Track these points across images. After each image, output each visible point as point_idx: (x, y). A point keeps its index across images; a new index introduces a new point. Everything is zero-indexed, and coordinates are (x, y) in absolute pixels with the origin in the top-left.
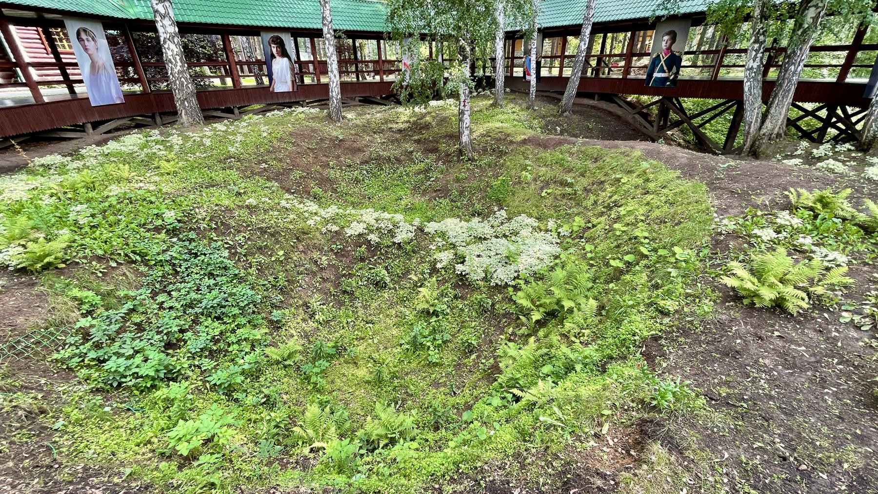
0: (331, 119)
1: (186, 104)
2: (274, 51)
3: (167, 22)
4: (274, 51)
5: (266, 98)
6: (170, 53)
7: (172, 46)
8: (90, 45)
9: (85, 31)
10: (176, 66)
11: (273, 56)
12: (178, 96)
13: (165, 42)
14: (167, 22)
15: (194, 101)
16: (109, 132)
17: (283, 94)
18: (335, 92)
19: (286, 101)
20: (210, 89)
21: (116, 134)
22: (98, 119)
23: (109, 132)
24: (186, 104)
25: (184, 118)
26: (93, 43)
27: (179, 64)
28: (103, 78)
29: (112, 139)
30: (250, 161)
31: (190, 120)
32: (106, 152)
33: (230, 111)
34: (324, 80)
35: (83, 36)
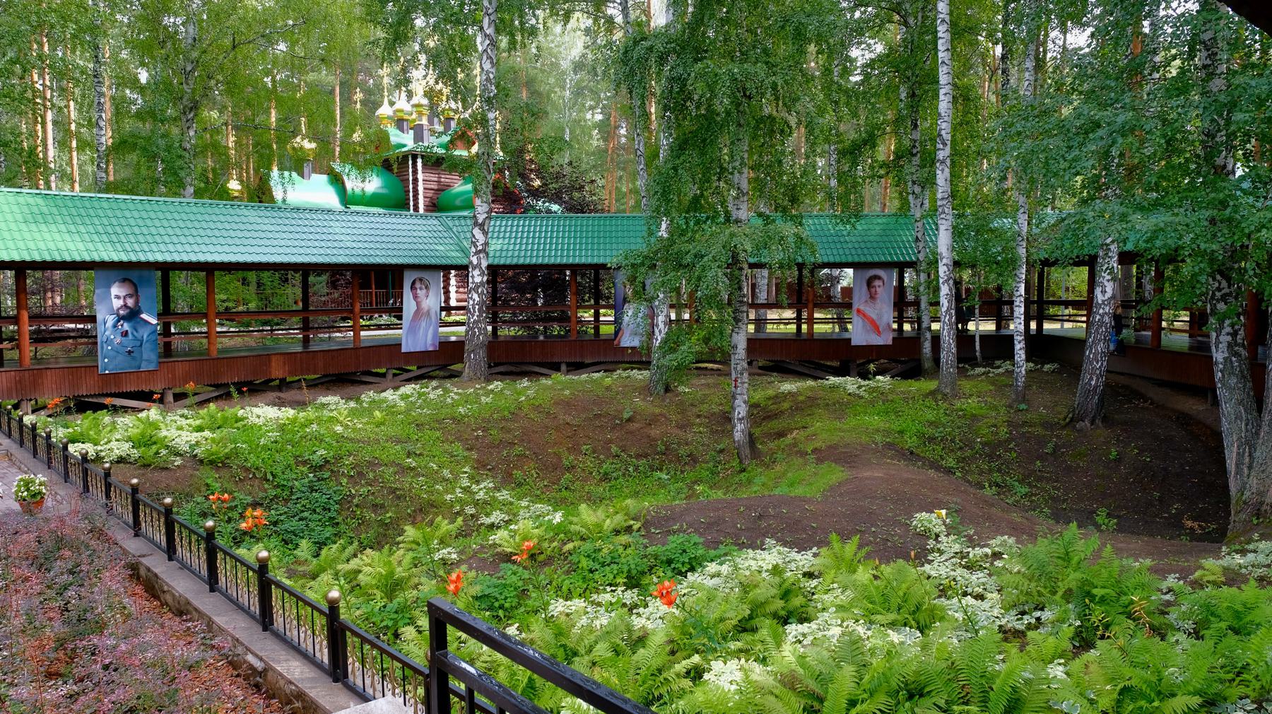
3: (476, 272)
8: (421, 293)
9: (421, 280)
14: (476, 272)
15: (482, 353)
28: (423, 324)
35: (418, 285)
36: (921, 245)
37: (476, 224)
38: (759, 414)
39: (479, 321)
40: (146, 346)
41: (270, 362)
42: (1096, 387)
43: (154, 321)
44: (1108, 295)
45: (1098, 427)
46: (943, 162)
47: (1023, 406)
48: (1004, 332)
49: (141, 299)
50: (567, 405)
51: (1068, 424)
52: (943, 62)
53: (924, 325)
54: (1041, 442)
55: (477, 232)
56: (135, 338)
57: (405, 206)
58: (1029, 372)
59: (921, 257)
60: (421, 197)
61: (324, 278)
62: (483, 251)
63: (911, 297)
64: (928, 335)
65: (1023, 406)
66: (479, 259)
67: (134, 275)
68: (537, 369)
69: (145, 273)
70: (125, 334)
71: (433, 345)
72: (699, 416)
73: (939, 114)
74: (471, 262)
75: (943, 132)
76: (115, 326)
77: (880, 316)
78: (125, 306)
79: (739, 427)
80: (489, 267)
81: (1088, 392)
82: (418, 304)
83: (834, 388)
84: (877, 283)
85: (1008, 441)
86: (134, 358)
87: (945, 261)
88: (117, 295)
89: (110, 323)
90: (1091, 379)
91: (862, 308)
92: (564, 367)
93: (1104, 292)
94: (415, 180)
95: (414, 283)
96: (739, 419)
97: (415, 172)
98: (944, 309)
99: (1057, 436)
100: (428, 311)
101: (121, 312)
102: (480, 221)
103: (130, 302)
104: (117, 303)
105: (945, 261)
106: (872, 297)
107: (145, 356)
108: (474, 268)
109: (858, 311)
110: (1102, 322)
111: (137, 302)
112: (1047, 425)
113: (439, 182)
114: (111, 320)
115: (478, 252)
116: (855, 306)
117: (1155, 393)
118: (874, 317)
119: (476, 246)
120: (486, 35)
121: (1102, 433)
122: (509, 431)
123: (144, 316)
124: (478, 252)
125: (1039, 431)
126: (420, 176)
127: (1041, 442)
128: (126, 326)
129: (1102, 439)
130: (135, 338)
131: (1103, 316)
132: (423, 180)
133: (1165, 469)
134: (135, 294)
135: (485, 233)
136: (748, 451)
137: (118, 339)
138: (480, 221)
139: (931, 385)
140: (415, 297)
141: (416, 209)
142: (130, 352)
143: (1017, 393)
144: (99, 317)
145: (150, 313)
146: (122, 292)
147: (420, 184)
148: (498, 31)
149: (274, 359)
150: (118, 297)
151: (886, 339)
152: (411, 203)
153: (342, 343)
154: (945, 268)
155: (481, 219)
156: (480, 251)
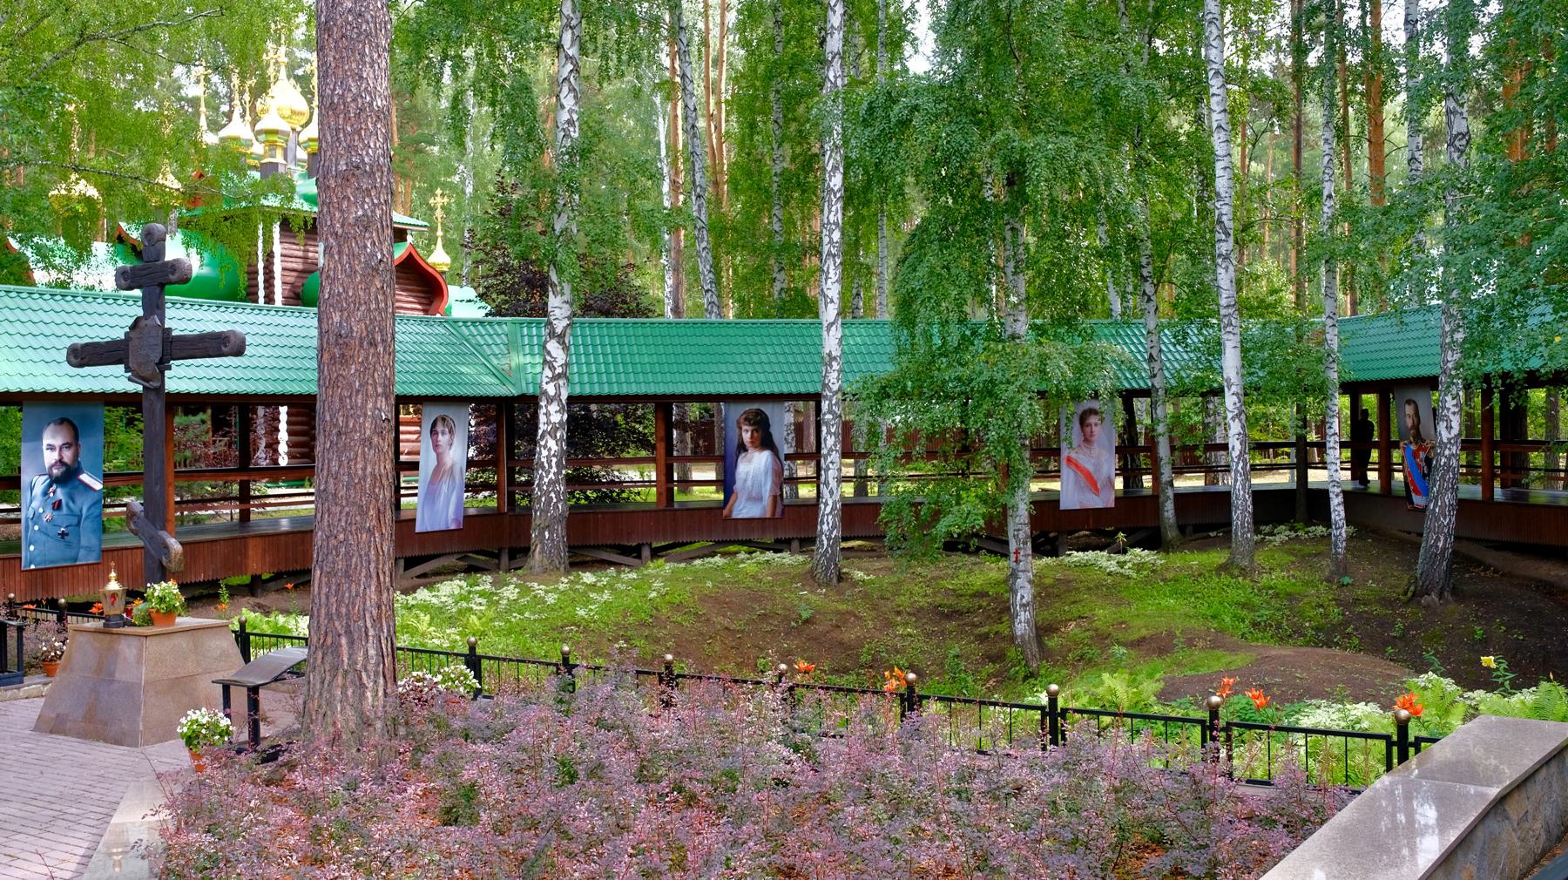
0: (813, 577)
1: (547, 537)
2: (747, 437)
3: (554, 407)
4: (747, 437)
5: (716, 528)
6: (545, 453)
7: (552, 444)
8: (443, 439)
9: (444, 419)
10: (548, 473)
11: (742, 448)
12: (538, 519)
13: (543, 436)
14: (554, 407)
15: (560, 529)
16: (424, 575)
17: (749, 521)
18: (1440, 531)
19: (750, 535)
20: (631, 508)
21: (433, 579)
22: (417, 553)
23: (424, 575)
24: (547, 537)
25: (537, 557)
26: (447, 436)
27: (554, 469)
28: (445, 488)
29: (425, 586)
30: (602, 634)
31: (546, 562)
32: (412, 602)
33: (635, 552)
34: (1316, 477)
35: (439, 428)
36: (1157, 366)
37: (552, 334)
38: (1046, 594)
39: (557, 481)
40: (85, 524)
41: (246, 548)
42: (1444, 549)
43: (98, 486)
44: (1455, 431)
45: (1448, 602)
46: (1226, 258)
47: (1346, 580)
48: (1220, 487)
49: (82, 451)
50: (719, 601)
51: (1410, 600)
52: (1219, 127)
53: (1165, 478)
54: (1385, 624)
55: (553, 346)
56: (71, 513)
57: (251, 296)
58: (1350, 538)
59: (1158, 382)
60: (278, 283)
61: (206, 416)
62: (563, 375)
63: (1142, 442)
64: (1170, 493)
65: (1346, 580)
66: (558, 388)
67: (72, 412)
68: (605, 556)
69: (91, 410)
70: (57, 506)
71: (456, 520)
72: (899, 613)
73: (1218, 194)
74: (545, 393)
75: (1224, 218)
76: (45, 493)
77: (1098, 466)
78: (61, 462)
79: (1023, 616)
80: (572, 400)
81: (1433, 558)
82: (439, 457)
83: (1086, 566)
84: (1093, 420)
85: (1346, 623)
86: (69, 545)
87: (1234, 389)
88: (51, 447)
89: (38, 490)
90: (1438, 539)
91: (1073, 455)
92: (795, 544)
93: (1449, 428)
94: (269, 256)
95: (434, 424)
96: (1023, 605)
97: (268, 241)
98: (1235, 453)
99: (1402, 616)
100: (452, 468)
101: (55, 471)
102: (559, 331)
103: (68, 456)
104: (50, 457)
105: (1234, 389)
106: (1087, 440)
107: (84, 542)
108: (550, 400)
109: (1069, 460)
110: (1448, 467)
111: (76, 455)
112: (1386, 602)
113: (306, 258)
114: (40, 483)
115: (555, 378)
116: (1065, 453)
117: (1493, 558)
118: (1090, 468)
119: (552, 368)
120: (568, 57)
121: (1455, 609)
122: (657, 641)
123: (84, 477)
124: (555, 378)
125: (1377, 609)
126: (277, 249)
127: (1385, 624)
128: (60, 494)
129: (1457, 616)
130: (71, 513)
131: (1449, 459)
132: (283, 255)
133: (1544, 648)
134: (73, 443)
135: (566, 348)
136: (1035, 649)
137: (48, 515)
138: (559, 331)
139: (1217, 557)
140: (436, 446)
141: (269, 299)
142: (63, 535)
143: (1337, 563)
144: (25, 479)
145: (94, 474)
146: (58, 442)
147: (277, 260)
148: (583, 51)
149: (251, 543)
150: (51, 448)
151: (1104, 501)
152: (261, 293)
153: (217, 529)
154: (1235, 399)
155: (559, 326)
156: (559, 376)
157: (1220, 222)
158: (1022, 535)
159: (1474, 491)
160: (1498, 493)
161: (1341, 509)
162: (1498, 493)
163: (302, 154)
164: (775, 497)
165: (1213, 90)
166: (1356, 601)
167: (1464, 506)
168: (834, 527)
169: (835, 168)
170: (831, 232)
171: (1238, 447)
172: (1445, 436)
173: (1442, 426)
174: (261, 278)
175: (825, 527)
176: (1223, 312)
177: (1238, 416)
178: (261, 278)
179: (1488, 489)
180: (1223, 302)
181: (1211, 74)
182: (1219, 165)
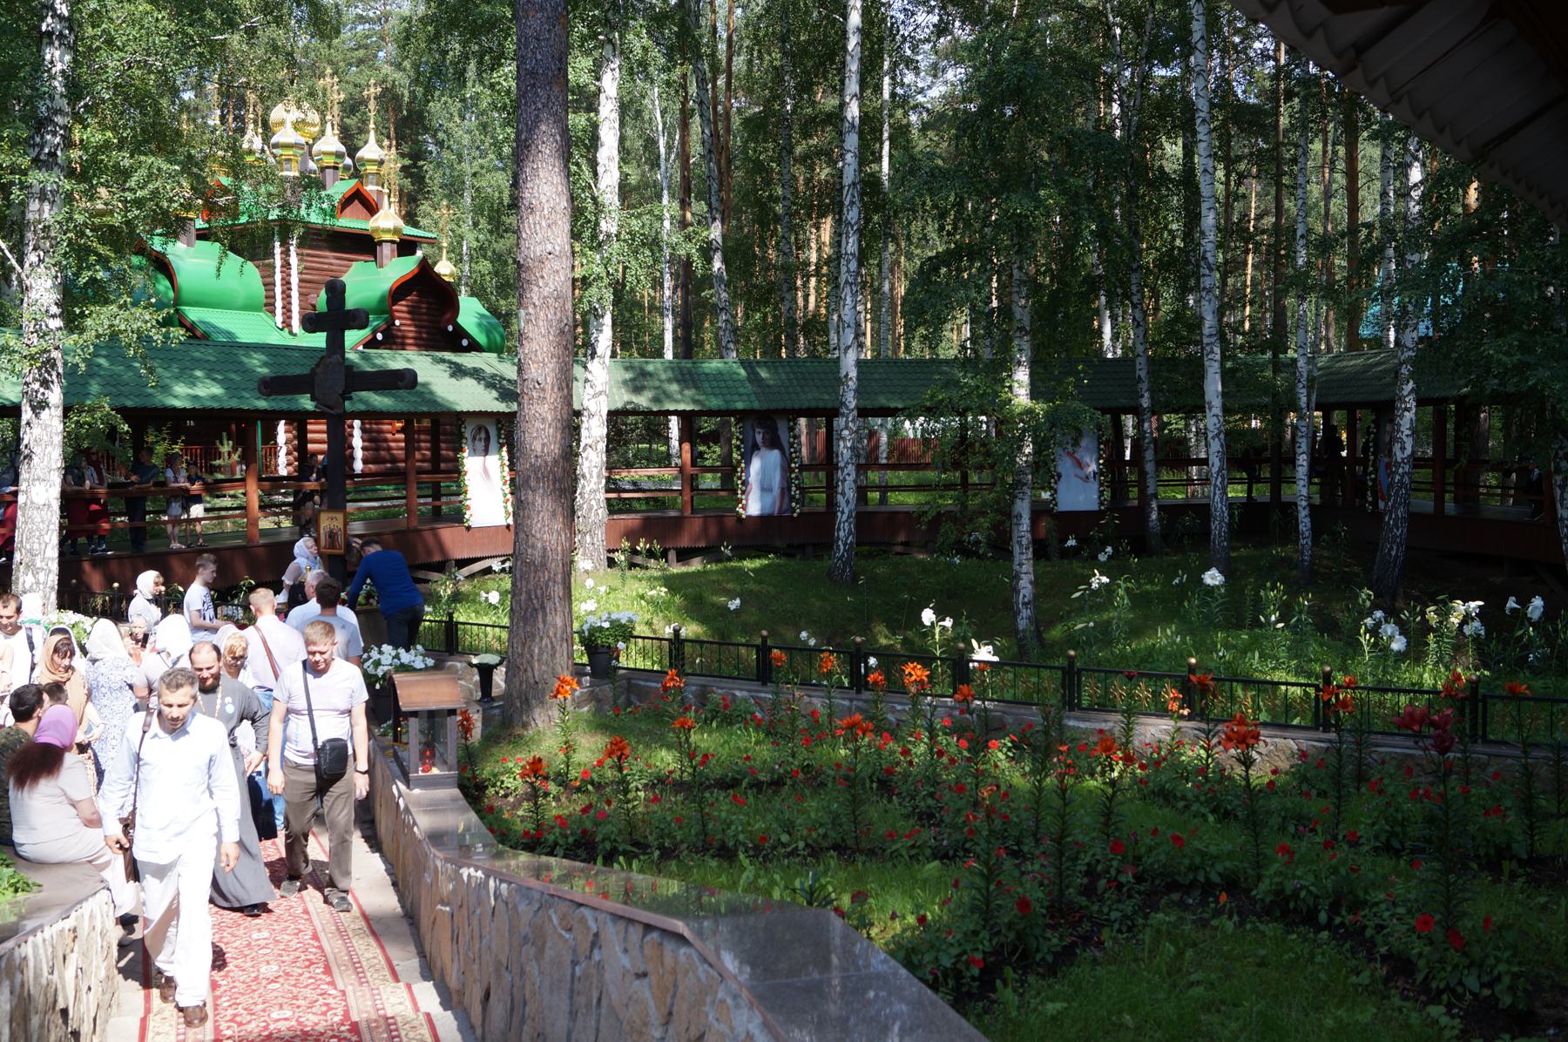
2: (759, 438)
4: (759, 438)
42: (1397, 556)
44: (1408, 451)
79: (1025, 613)
93: (1403, 449)
98: (1215, 470)
131: (1402, 476)
157: (1204, 258)
158: (1024, 541)
159: (1424, 503)
160: (1450, 507)
161: (1307, 520)
162: (1450, 507)
163: (56, 323)
164: (782, 489)
165: (1200, 137)
166: (1143, 474)
167: (1414, 519)
168: (850, 533)
169: (852, 203)
170: (848, 261)
171: (1217, 463)
172: (1399, 456)
173: (1397, 447)
174: (278, 290)
175: (842, 534)
176: (1205, 340)
177: (1217, 435)
178: (278, 290)
179: (1439, 501)
180: (1206, 331)
181: (1198, 121)
182: (1205, 206)
